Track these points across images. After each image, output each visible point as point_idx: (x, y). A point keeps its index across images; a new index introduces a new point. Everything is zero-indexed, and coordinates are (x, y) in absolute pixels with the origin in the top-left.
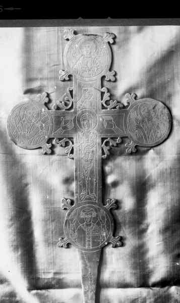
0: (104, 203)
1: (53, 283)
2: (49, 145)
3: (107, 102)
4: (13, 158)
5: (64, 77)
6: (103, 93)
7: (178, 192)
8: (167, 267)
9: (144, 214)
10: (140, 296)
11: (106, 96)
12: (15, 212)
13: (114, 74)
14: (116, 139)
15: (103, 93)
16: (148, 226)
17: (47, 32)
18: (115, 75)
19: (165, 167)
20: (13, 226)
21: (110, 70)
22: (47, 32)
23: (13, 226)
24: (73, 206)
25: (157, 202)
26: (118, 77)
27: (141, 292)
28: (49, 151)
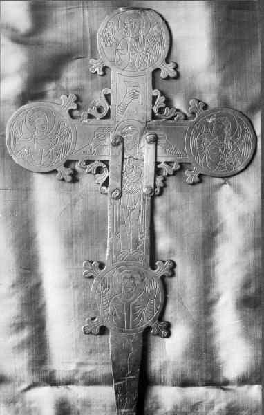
0: (153, 267)
1: (76, 378)
2: (69, 171)
3: (161, 110)
4: (7, 28)
5: (97, 69)
6: (154, 98)
7: (260, 346)
8: (247, 357)
9: (219, 24)
10: (205, 398)
11: (161, 100)
12: (18, 275)
13: (174, 66)
14: (172, 164)
15: (154, 98)
16: (219, 296)
17: (67, 9)
18: (176, 68)
19: (247, 212)
20: (16, 296)
21: (167, 60)
22: (67, 9)
23: (16, 296)
24: (103, 270)
25: (234, 262)
26: (180, 69)
27: (207, 393)
28: (69, 178)
